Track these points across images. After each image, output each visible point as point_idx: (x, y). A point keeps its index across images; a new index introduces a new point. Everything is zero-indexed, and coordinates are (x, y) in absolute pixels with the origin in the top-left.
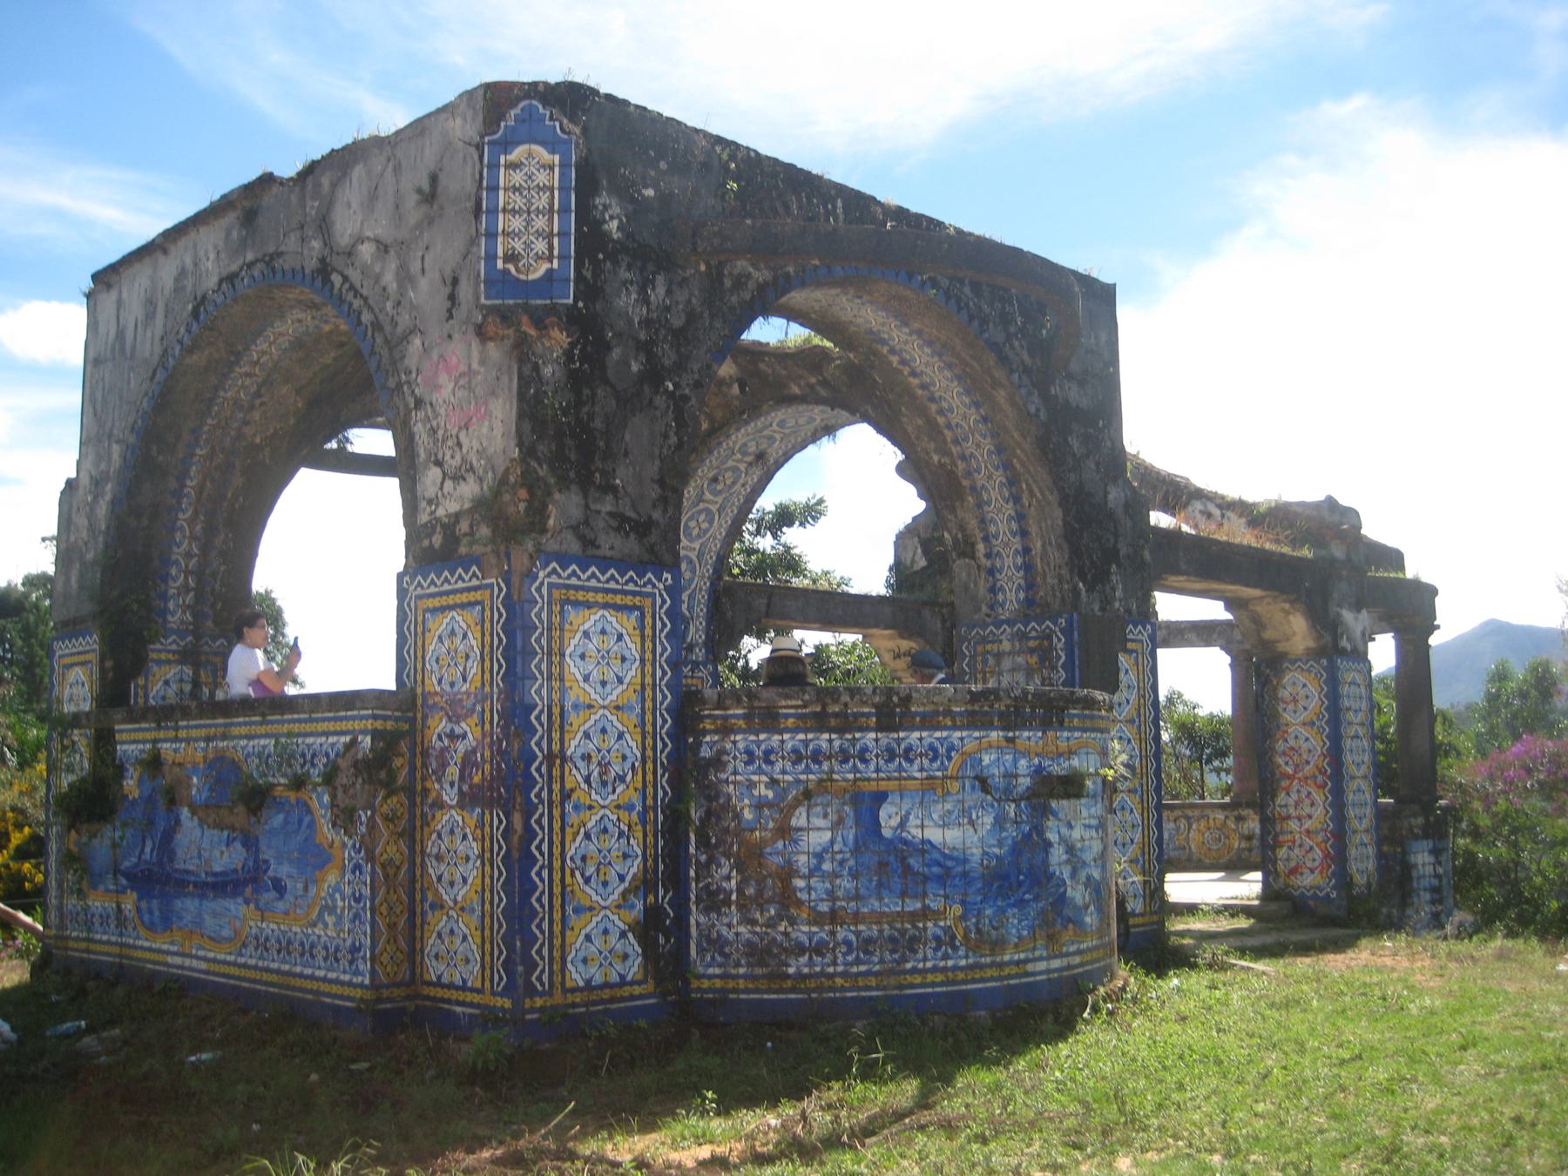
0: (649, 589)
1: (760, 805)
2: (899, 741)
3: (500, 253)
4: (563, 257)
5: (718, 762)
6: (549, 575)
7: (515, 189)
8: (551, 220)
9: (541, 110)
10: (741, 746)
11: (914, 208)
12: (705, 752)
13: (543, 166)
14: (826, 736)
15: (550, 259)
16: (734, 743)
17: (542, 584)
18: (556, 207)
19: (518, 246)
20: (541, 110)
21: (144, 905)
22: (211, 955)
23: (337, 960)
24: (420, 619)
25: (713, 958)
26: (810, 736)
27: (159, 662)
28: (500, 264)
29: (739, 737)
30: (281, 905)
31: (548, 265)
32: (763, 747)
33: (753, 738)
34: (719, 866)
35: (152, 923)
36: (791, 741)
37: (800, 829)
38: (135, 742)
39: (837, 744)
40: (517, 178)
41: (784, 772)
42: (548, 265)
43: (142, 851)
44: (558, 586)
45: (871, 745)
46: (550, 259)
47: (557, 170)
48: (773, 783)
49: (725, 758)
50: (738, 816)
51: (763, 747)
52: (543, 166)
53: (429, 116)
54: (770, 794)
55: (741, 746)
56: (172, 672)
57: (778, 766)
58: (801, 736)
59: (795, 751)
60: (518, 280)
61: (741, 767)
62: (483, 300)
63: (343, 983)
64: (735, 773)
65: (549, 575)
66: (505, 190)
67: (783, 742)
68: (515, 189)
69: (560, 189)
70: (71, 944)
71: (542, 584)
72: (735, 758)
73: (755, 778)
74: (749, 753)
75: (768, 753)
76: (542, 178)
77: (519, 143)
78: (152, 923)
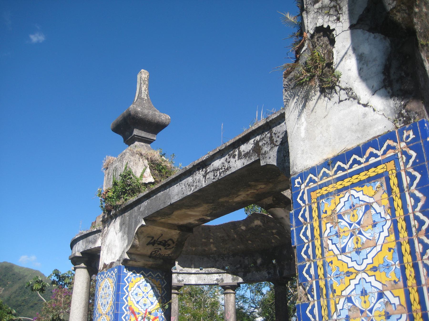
0: (306, 197)
44: (314, 190)
65: (404, 153)
71: (303, 193)
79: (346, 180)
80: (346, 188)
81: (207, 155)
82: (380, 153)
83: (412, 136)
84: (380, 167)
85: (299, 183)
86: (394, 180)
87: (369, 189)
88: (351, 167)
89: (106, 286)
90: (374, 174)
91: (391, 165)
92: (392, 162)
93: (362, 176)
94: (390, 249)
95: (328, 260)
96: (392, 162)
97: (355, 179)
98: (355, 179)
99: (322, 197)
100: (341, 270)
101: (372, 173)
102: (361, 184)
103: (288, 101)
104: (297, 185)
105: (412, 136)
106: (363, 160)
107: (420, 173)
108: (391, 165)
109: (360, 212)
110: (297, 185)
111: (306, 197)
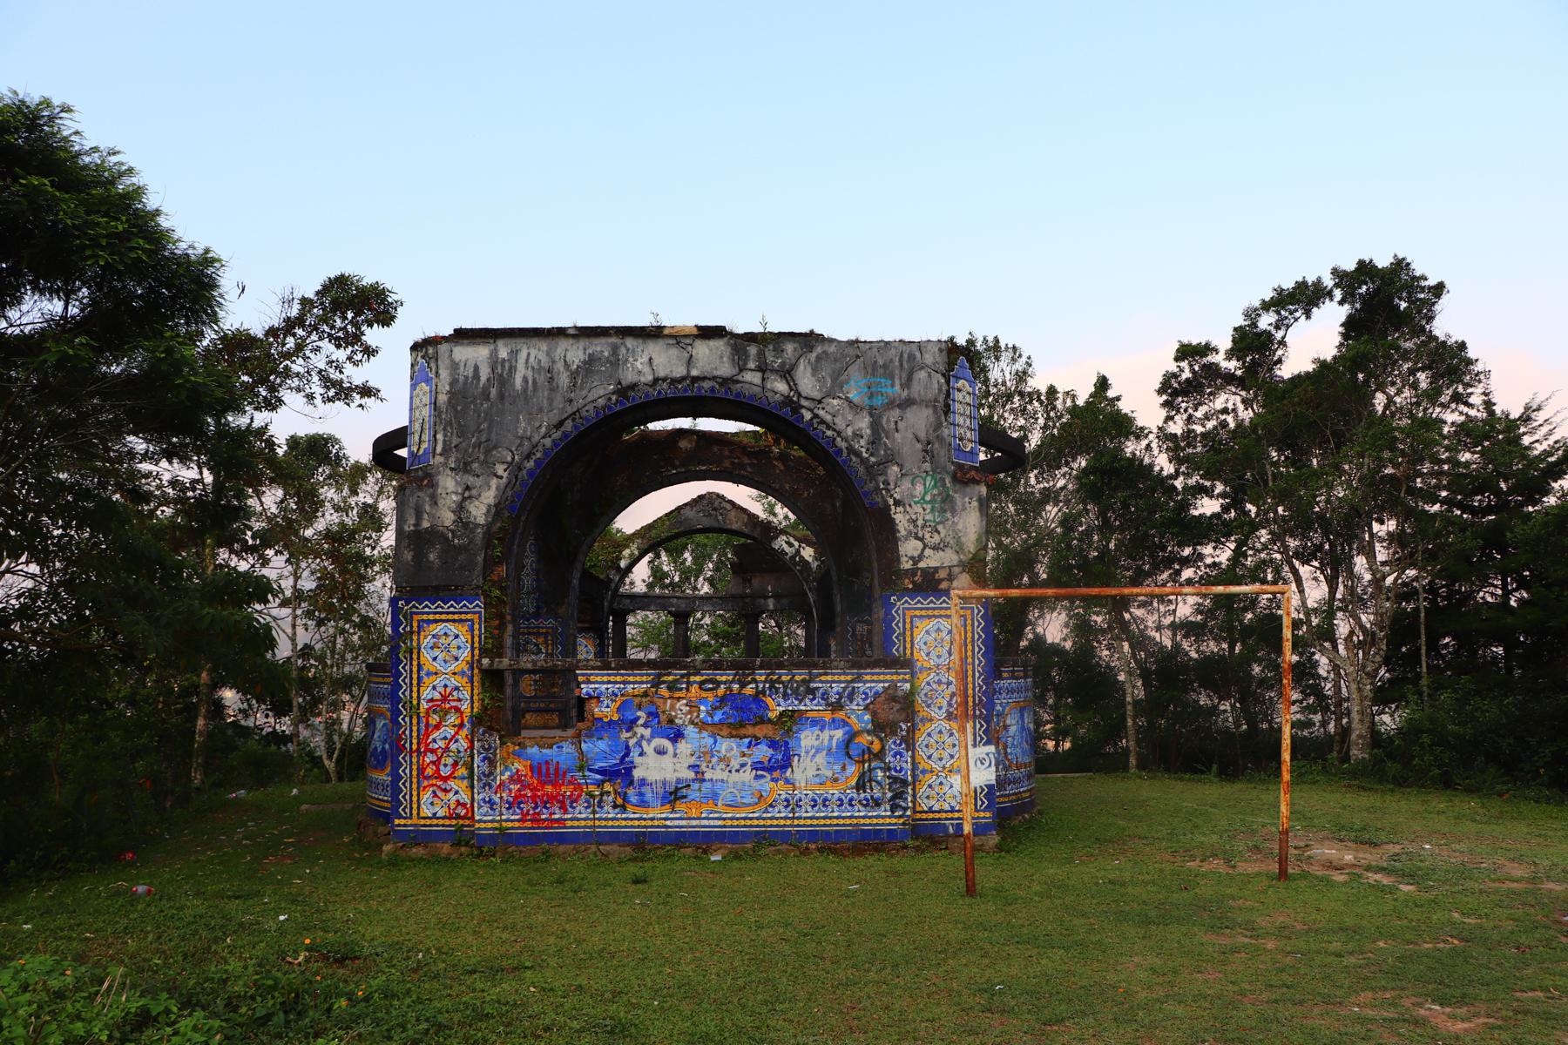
93: (456, 617)
97: (450, 617)
98: (450, 617)
102: (454, 621)
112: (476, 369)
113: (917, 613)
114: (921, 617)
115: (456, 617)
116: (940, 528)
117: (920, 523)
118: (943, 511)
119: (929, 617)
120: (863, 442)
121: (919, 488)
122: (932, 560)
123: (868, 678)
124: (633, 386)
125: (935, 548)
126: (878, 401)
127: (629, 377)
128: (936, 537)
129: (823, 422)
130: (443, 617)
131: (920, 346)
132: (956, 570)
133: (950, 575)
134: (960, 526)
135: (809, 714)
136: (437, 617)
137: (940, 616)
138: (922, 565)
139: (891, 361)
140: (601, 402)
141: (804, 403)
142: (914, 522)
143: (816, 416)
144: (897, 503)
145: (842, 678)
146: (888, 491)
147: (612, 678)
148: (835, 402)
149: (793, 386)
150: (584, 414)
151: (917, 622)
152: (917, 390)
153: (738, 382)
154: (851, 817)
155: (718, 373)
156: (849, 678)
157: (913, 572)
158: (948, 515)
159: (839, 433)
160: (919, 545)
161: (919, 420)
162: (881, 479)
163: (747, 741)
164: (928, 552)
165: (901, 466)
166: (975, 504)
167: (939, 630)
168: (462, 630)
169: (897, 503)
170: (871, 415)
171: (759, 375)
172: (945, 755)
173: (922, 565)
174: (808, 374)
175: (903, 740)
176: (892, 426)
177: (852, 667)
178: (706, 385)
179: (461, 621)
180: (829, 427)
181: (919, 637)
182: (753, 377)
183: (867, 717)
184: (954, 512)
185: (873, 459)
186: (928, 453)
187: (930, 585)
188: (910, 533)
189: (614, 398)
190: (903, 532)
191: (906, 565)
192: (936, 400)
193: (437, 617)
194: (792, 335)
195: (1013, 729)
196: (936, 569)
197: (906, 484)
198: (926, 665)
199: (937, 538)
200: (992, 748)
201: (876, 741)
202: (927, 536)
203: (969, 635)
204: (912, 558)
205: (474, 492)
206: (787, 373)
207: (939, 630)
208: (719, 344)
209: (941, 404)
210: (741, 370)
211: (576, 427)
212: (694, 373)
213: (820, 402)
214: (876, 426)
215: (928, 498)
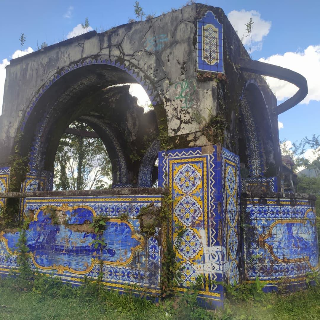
0: (167, 162)
1: (263, 227)
2: (262, 208)
3: (203, 56)
4: (220, 60)
5: (251, 214)
6: (210, 156)
7: (206, 37)
8: (217, 48)
9: (213, 15)
10: (258, 209)
11: (5, 80)
12: (248, 211)
13: (214, 31)
14: (279, 207)
15: (217, 59)
16: (256, 208)
17: (166, 160)
18: (218, 44)
19: (208, 54)
20: (213, 15)
21: (38, 257)
22: (74, 275)
23: (11, 263)
24: (171, 166)
25: (252, 274)
26: (276, 207)
27: (30, 179)
28: (203, 59)
29: (257, 206)
30: (112, 259)
31: (216, 61)
32: (264, 209)
33: (261, 206)
34: (253, 245)
35: (42, 263)
36: (271, 208)
37: (275, 234)
38: (36, 203)
39: (282, 209)
40: (207, 33)
41: (269, 217)
42: (216, 61)
43: (39, 238)
44: (171, 159)
45: (290, 209)
46: (217, 59)
47: (218, 33)
48: (267, 220)
49: (253, 212)
50: (257, 230)
51: (264, 209)
52: (214, 31)
53: (206, 6)
54: (266, 224)
55: (270, 209)
56: (33, 182)
57: (268, 215)
58: (273, 207)
59: (272, 211)
60: (208, 64)
61: (258, 215)
62: (198, 69)
63: (4, 268)
64: (256, 217)
65: (210, 156)
66: (204, 36)
67: (269, 208)
68: (206, 37)
69: (219, 39)
70: (105, 284)
71: (166, 160)
72: (256, 212)
73: (262, 218)
74: (260, 211)
75: (265, 211)
76: (214, 35)
77: (207, 23)
78: (42, 263)
79: (186, 160)
80: (186, 163)
81: (215, 111)
82: (180, 155)
83: (164, 153)
84: (200, 158)
85: (164, 155)
86: (205, 165)
87: (195, 165)
88: (175, 156)
89: (232, 204)
90: (198, 160)
91: (205, 159)
92: (206, 158)
93: (193, 160)
94: (200, 189)
95: (174, 189)
96: (206, 158)
97: (190, 160)
98: (190, 160)
99: (175, 163)
100: (179, 193)
101: (197, 160)
102: (192, 162)
103: (193, 115)
104: (163, 156)
105: (164, 153)
106: (180, 155)
107: (214, 164)
108: (205, 159)
109: (190, 173)
110: (163, 156)
111: (167, 162)
112: (16, 74)
113: (176, 161)
114: (178, 164)
115: (193, 160)
116: (190, 110)
117: (179, 109)
118: (191, 100)
119: (182, 163)
120: (152, 71)
121: (179, 90)
122: (185, 130)
123: (139, 199)
124: (63, 69)
125: (187, 123)
126: (160, 47)
127: (61, 65)
128: (187, 115)
129: (134, 65)
130: (186, 160)
131: (204, 5)
132: (198, 134)
133: (195, 137)
134: (201, 108)
135: (112, 220)
136: (183, 161)
137: (188, 163)
138: (179, 133)
139: (167, 23)
140: (52, 78)
141: (126, 58)
142: (176, 109)
143: (131, 63)
144: (168, 100)
145: (127, 200)
146: (163, 94)
147: (37, 201)
148: (139, 53)
149: (122, 52)
150: (46, 84)
151: (176, 167)
152: (179, 35)
153: (100, 55)
154: (115, 283)
155: (92, 54)
156: (130, 199)
157: (175, 137)
158: (194, 102)
159: (141, 69)
160: (178, 122)
161: (180, 52)
162: (160, 88)
163: (83, 234)
164: (183, 125)
165: (170, 79)
166: (210, 93)
167: (187, 171)
168: (179, 169)
169: (168, 100)
170: (156, 56)
171: (108, 50)
172: (191, 250)
173: (179, 133)
174: (128, 43)
175: (157, 239)
176: (167, 58)
177: (132, 194)
178: (88, 60)
179: (196, 162)
180: (136, 67)
181: (177, 174)
182: (106, 52)
183: (138, 223)
184: (198, 100)
185: (156, 79)
186: (184, 69)
187: (182, 143)
188: (173, 116)
189: (56, 75)
190: (170, 116)
191: (171, 134)
192: (189, 38)
193: (183, 161)
194: (123, 26)
195: (279, 237)
196: (187, 135)
197: (172, 89)
198: (180, 193)
199: (188, 117)
200: (220, 248)
201: (142, 238)
202: (183, 116)
203: (205, 173)
204: (174, 130)
205: (12, 124)
206: (119, 46)
207: (187, 171)
208: (94, 41)
209: (192, 40)
210: (101, 49)
211: (43, 91)
212: (84, 56)
213: (133, 55)
214: (159, 62)
215: (183, 95)
